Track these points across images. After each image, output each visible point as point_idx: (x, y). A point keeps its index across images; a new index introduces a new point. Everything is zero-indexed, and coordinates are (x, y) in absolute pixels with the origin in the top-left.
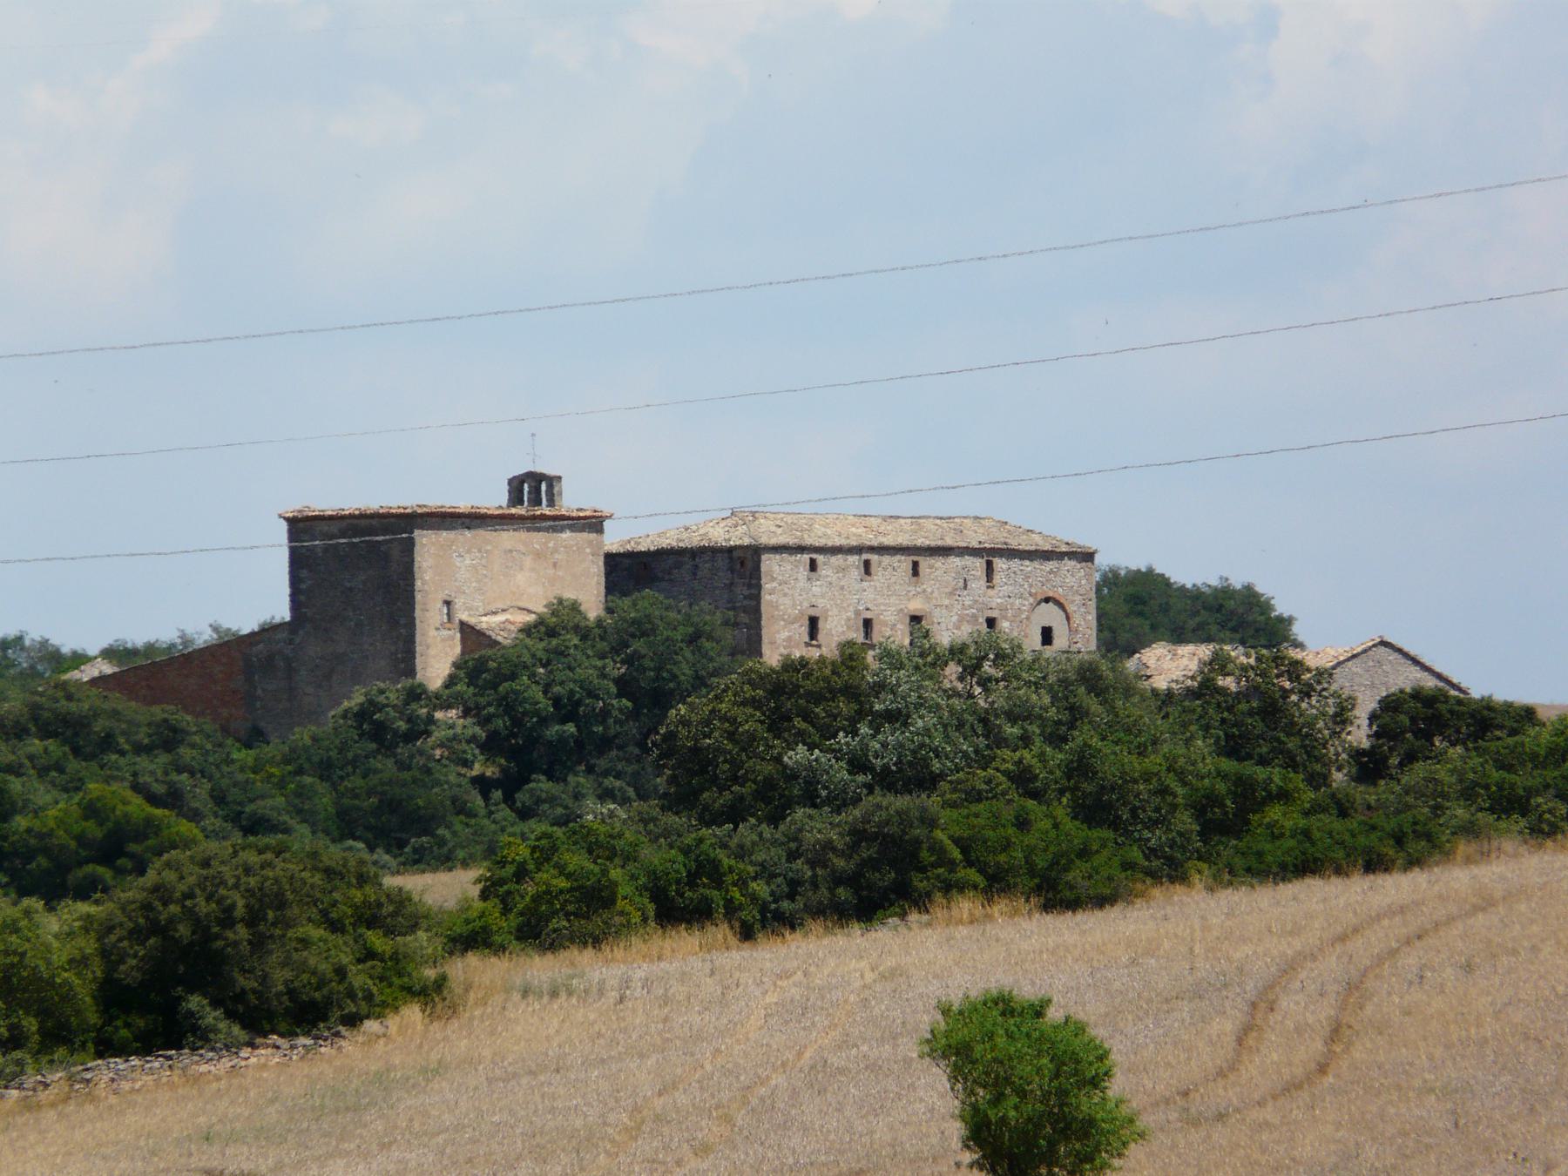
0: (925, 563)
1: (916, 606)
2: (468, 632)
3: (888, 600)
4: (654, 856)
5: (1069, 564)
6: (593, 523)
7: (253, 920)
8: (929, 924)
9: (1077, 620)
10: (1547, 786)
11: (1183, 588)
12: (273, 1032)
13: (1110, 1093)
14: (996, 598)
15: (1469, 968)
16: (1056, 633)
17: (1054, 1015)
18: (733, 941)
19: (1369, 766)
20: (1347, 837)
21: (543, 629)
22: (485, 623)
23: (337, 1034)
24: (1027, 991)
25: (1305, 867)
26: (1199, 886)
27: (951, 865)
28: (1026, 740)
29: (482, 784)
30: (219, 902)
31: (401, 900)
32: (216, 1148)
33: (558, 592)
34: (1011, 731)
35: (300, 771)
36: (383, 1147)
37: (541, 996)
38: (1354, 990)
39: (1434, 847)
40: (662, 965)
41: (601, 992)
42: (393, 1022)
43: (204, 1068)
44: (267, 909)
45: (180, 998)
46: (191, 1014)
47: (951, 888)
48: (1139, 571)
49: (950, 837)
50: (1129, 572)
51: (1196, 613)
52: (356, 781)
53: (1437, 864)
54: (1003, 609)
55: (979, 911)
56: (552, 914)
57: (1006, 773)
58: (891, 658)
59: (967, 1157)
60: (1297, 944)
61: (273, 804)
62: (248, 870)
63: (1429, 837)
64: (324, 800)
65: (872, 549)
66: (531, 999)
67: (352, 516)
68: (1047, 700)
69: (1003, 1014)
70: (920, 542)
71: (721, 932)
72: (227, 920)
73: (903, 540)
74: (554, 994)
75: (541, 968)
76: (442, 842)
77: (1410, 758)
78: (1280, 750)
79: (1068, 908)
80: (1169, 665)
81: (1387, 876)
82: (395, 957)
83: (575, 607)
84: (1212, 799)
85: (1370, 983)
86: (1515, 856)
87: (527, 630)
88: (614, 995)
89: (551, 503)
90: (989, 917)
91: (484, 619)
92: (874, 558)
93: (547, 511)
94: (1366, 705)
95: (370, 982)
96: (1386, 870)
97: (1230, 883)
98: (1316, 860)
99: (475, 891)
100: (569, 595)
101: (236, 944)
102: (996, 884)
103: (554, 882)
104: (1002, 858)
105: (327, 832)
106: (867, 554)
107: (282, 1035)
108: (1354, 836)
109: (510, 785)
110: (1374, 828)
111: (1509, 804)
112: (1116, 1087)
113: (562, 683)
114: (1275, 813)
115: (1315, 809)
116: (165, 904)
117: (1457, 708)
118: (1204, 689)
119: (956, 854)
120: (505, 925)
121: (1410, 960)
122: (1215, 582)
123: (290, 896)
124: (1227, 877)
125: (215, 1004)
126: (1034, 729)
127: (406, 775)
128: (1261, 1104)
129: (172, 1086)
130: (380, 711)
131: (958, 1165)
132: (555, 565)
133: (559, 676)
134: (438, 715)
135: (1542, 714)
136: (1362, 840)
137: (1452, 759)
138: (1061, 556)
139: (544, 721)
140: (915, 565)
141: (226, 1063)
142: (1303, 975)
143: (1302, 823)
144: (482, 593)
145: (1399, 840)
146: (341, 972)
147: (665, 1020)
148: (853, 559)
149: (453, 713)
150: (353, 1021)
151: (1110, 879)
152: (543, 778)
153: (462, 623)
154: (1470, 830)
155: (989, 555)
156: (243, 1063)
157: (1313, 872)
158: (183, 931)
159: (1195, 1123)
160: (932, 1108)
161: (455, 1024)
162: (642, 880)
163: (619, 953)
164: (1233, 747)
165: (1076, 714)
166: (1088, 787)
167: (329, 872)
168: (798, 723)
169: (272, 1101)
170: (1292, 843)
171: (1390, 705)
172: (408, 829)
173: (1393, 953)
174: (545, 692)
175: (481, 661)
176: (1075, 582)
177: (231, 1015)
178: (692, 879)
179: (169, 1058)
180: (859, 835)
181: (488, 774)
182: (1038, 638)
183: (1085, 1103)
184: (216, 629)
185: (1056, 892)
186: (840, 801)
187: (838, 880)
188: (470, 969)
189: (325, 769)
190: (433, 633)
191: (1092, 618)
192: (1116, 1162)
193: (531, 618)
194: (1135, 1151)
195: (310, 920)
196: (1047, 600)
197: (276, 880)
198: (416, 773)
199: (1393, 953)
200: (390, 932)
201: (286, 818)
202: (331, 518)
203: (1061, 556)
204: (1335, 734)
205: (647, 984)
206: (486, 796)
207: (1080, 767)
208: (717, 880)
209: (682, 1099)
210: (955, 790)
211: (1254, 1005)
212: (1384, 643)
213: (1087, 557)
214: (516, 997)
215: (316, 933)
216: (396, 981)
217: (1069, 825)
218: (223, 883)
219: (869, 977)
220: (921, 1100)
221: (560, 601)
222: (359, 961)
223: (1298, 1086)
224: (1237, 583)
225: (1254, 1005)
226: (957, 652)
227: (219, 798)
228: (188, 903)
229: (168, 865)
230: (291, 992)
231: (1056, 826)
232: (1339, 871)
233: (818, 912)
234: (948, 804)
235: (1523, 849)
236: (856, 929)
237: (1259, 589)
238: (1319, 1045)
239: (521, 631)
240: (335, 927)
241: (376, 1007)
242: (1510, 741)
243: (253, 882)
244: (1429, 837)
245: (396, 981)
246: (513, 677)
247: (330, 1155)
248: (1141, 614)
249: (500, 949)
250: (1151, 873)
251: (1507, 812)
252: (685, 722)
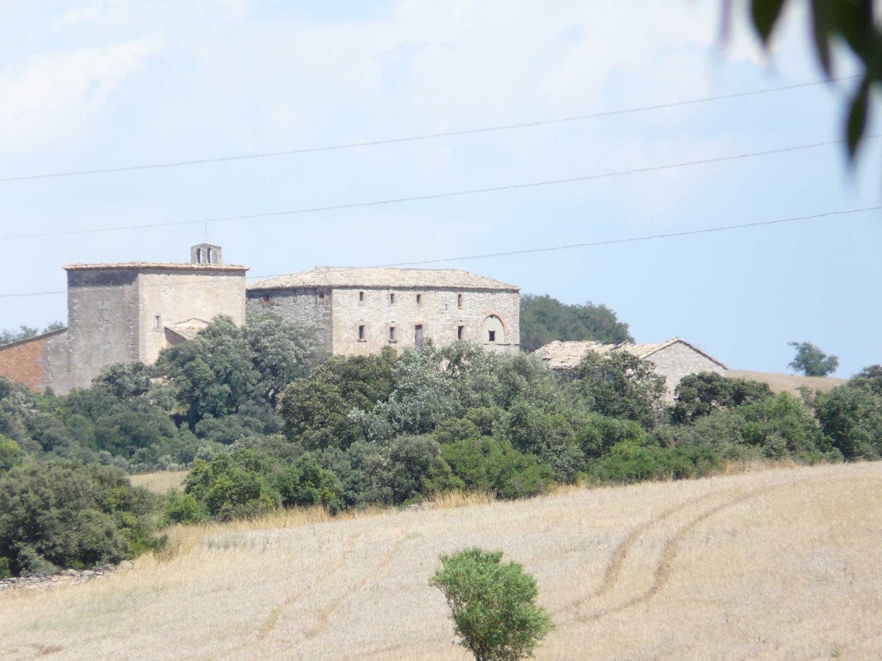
0: (425, 295)
1: (418, 320)
2: (171, 335)
3: (404, 313)
4: (281, 469)
5: (505, 295)
6: (241, 272)
7: (60, 505)
8: (433, 507)
9: (508, 326)
10: (775, 430)
11: (566, 307)
12: (71, 567)
13: (536, 604)
14: (463, 314)
15: (733, 534)
16: (496, 336)
17: (505, 561)
18: (326, 516)
19: (677, 416)
20: (665, 459)
21: (210, 332)
22: (180, 328)
23: (106, 568)
24: (488, 547)
25: (642, 475)
26: (583, 486)
27: (446, 474)
28: (484, 402)
29: (177, 420)
30: (41, 495)
31: (142, 494)
32: (39, 633)
33: (219, 312)
34: (475, 396)
35: (74, 412)
36: (133, 631)
37: (219, 548)
38: (670, 547)
39: (713, 464)
40: (286, 529)
41: (253, 545)
42: (138, 562)
43: (33, 586)
44: (66, 498)
45: (19, 549)
46: (25, 557)
47: (446, 487)
48: (542, 297)
49: (446, 460)
50: (536, 297)
51: (574, 321)
52: (106, 417)
53: (715, 475)
54: (467, 320)
55: (461, 501)
56: (224, 501)
57: (474, 421)
58: (408, 358)
59: (458, 639)
60: (638, 520)
61: (57, 431)
62: (58, 478)
63: (710, 458)
64: (89, 429)
65: (395, 288)
66: (213, 549)
67: (104, 269)
68: (495, 378)
69: (476, 560)
70: (422, 283)
71: (319, 511)
72: (46, 507)
73: (412, 283)
74: (226, 547)
75: (219, 532)
76: (154, 452)
77: (699, 413)
78: (625, 407)
79: (509, 498)
80: (565, 354)
81: (687, 481)
82: (138, 527)
83: (229, 320)
84: (591, 438)
85: (680, 543)
86: (758, 470)
87: (202, 333)
88: (259, 548)
89: (216, 261)
90: (466, 504)
91: (179, 325)
92: (396, 292)
93: (213, 266)
94: (672, 383)
95: (125, 539)
96: (687, 477)
97: (602, 484)
98: (648, 472)
99: (182, 489)
100: (226, 313)
101: (51, 518)
102: (470, 485)
103: (226, 483)
104: (474, 471)
105: (90, 446)
106: (393, 290)
107: (75, 569)
108: (669, 458)
109: (193, 418)
110: (680, 454)
111: (756, 439)
112: (539, 600)
113: (221, 362)
114: (624, 446)
115: (649, 442)
116: (13, 495)
117: (724, 384)
118: (582, 373)
119: (448, 468)
120: (198, 507)
121: (702, 529)
122: (583, 304)
123: (81, 493)
124: (599, 481)
125: (40, 551)
126: (489, 396)
127: (135, 414)
128: (618, 610)
129: (14, 597)
130: (119, 377)
131: (453, 642)
132: (217, 295)
133: (219, 359)
134: (153, 381)
135: (772, 388)
136: (674, 461)
137: (722, 413)
138: (501, 291)
139: (209, 384)
140: (418, 297)
141: (46, 584)
142: (642, 537)
143: (639, 451)
144: (178, 311)
145: (695, 461)
146: (109, 534)
147: (289, 561)
148: (384, 292)
149: (160, 380)
150: (115, 561)
151: (534, 482)
152: (211, 415)
153: (166, 329)
154: (733, 455)
155: (458, 290)
156: (54, 584)
157: (646, 479)
158: (21, 511)
159: (581, 620)
160: (438, 610)
161: (172, 563)
162: (275, 482)
163: (262, 523)
164: (602, 406)
165: (515, 389)
166: (523, 431)
167: (102, 480)
168: (357, 394)
169: (71, 607)
170: (635, 462)
171: (687, 382)
172: (134, 443)
173: (692, 525)
174: (211, 368)
175: (178, 355)
176: (509, 307)
177: (48, 558)
178: (303, 479)
179: (14, 582)
180: (395, 457)
181: (181, 412)
182: (488, 337)
183: (523, 608)
184: (24, 329)
185: (503, 490)
186: (382, 439)
187: (383, 482)
188: (176, 532)
189: (88, 411)
190: (149, 333)
191: (517, 326)
192: (539, 642)
193: (204, 326)
194: (550, 637)
195: (91, 507)
196: (492, 316)
197: (74, 483)
198: (142, 413)
199: (692, 525)
200: (137, 513)
201: (66, 438)
202: (91, 269)
203: (501, 291)
204: (656, 397)
205: (278, 541)
206: (178, 426)
207: (519, 420)
208: (316, 480)
209: (298, 605)
210: (445, 430)
211: (614, 553)
212: (680, 342)
213: (517, 291)
214: (205, 548)
215: (94, 513)
216: (140, 540)
217: (513, 453)
218: (45, 485)
219: (402, 537)
220: (430, 606)
221: (221, 317)
222: (119, 528)
223: (639, 600)
224: (596, 304)
225: (614, 553)
226: (446, 353)
227: (30, 427)
228: (24, 495)
229: (12, 476)
230: (80, 545)
231: (504, 453)
232: (661, 479)
233: (371, 501)
234: (442, 440)
235: (763, 466)
236: (394, 510)
237: (608, 307)
238: (651, 578)
239: (199, 333)
240: (107, 510)
241: (130, 554)
242: (755, 404)
243: (60, 484)
244: (710, 458)
245: (140, 540)
246: (192, 359)
247: (104, 637)
248: (544, 322)
249: (196, 521)
250: (556, 479)
251: (754, 443)
252: (295, 392)
